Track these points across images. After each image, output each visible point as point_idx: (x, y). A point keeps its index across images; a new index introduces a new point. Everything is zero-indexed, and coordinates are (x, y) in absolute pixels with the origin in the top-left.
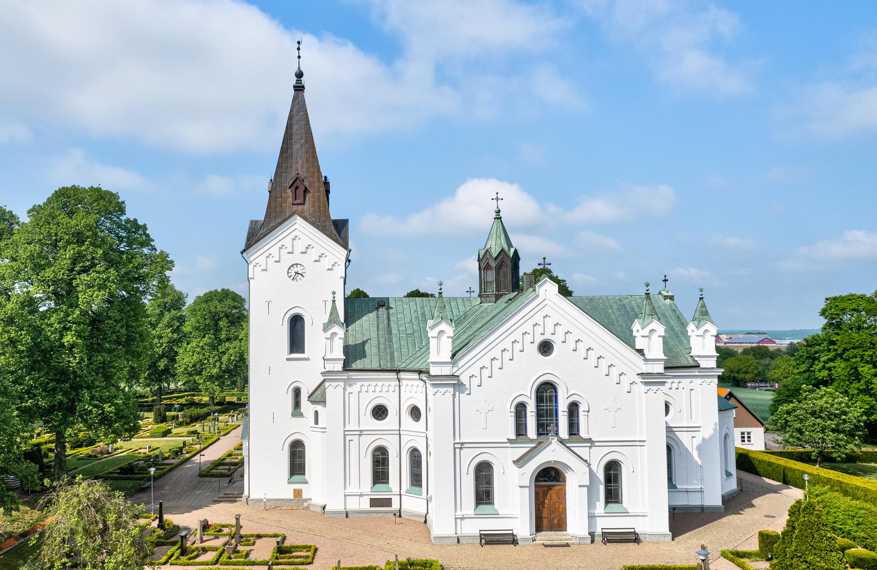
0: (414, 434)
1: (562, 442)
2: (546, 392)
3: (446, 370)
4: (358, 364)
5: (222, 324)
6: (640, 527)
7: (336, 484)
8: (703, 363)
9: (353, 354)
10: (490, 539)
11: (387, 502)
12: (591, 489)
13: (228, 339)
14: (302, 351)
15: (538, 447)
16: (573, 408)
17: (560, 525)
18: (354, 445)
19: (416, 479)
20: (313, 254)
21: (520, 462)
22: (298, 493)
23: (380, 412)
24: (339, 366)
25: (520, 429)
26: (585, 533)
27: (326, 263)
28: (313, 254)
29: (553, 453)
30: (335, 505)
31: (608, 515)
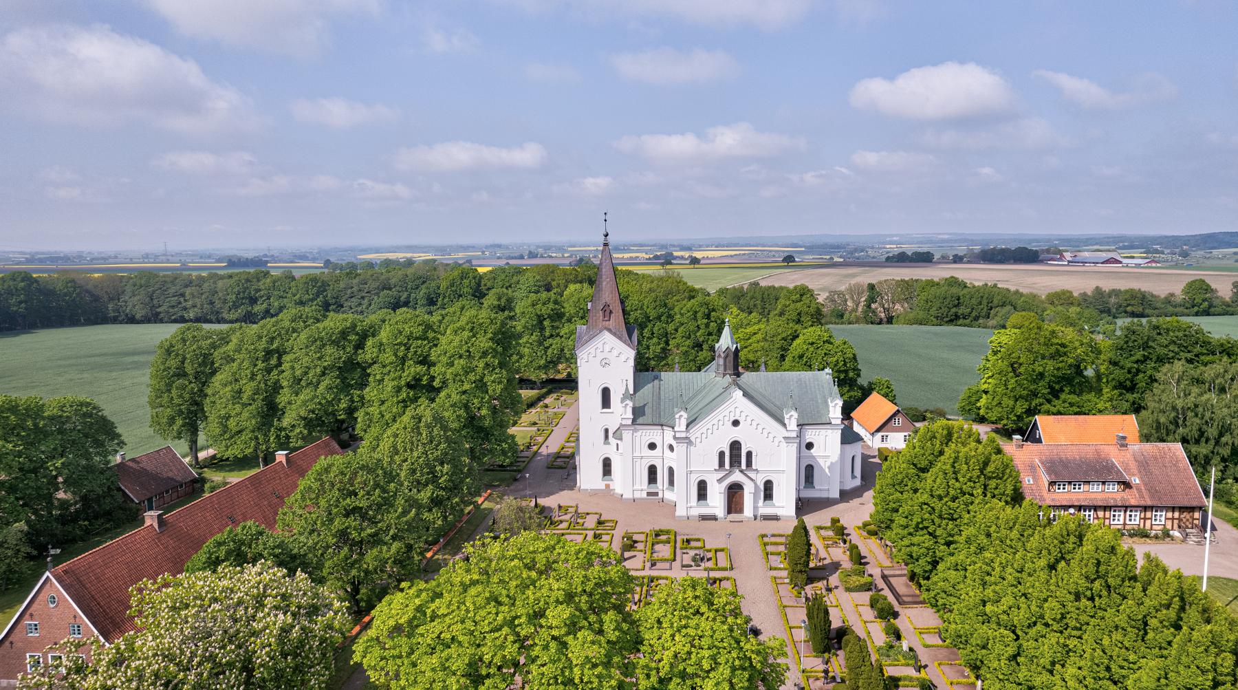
0: (671, 459)
1: (742, 471)
2: (735, 446)
3: (683, 435)
4: (640, 420)
5: (546, 323)
6: (780, 512)
7: (628, 483)
8: (833, 422)
9: (638, 412)
10: (704, 518)
11: (656, 494)
12: (756, 495)
13: (552, 336)
14: (609, 407)
15: (730, 473)
16: (749, 454)
17: (741, 511)
18: (638, 464)
19: (671, 482)
20: (615, 353)
21: (720, 481)
22: (608, 486)
23: (652, 446)
24: (630, 422)
25: (722, 464)
26: (751, 515)
27: (623, 358)
28: (615, 353)
29: (737, 477)
30: (628, 495)
31: (764, 506)
